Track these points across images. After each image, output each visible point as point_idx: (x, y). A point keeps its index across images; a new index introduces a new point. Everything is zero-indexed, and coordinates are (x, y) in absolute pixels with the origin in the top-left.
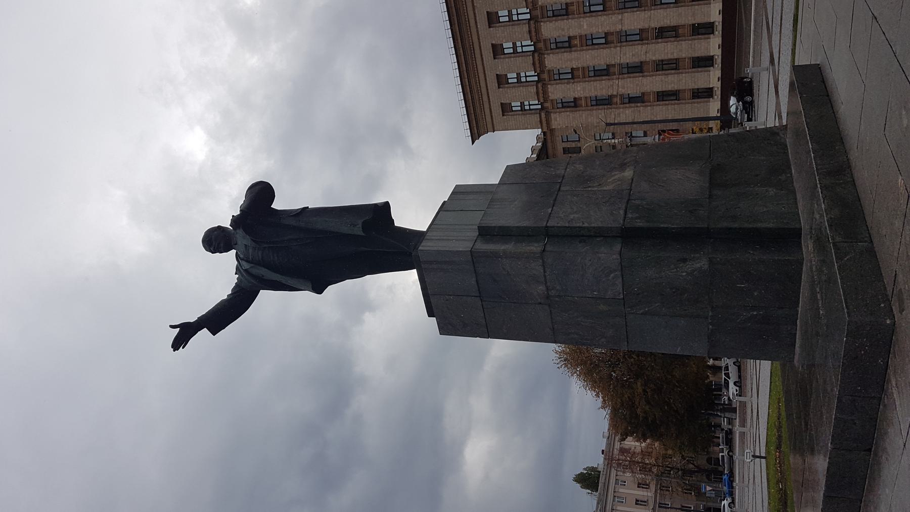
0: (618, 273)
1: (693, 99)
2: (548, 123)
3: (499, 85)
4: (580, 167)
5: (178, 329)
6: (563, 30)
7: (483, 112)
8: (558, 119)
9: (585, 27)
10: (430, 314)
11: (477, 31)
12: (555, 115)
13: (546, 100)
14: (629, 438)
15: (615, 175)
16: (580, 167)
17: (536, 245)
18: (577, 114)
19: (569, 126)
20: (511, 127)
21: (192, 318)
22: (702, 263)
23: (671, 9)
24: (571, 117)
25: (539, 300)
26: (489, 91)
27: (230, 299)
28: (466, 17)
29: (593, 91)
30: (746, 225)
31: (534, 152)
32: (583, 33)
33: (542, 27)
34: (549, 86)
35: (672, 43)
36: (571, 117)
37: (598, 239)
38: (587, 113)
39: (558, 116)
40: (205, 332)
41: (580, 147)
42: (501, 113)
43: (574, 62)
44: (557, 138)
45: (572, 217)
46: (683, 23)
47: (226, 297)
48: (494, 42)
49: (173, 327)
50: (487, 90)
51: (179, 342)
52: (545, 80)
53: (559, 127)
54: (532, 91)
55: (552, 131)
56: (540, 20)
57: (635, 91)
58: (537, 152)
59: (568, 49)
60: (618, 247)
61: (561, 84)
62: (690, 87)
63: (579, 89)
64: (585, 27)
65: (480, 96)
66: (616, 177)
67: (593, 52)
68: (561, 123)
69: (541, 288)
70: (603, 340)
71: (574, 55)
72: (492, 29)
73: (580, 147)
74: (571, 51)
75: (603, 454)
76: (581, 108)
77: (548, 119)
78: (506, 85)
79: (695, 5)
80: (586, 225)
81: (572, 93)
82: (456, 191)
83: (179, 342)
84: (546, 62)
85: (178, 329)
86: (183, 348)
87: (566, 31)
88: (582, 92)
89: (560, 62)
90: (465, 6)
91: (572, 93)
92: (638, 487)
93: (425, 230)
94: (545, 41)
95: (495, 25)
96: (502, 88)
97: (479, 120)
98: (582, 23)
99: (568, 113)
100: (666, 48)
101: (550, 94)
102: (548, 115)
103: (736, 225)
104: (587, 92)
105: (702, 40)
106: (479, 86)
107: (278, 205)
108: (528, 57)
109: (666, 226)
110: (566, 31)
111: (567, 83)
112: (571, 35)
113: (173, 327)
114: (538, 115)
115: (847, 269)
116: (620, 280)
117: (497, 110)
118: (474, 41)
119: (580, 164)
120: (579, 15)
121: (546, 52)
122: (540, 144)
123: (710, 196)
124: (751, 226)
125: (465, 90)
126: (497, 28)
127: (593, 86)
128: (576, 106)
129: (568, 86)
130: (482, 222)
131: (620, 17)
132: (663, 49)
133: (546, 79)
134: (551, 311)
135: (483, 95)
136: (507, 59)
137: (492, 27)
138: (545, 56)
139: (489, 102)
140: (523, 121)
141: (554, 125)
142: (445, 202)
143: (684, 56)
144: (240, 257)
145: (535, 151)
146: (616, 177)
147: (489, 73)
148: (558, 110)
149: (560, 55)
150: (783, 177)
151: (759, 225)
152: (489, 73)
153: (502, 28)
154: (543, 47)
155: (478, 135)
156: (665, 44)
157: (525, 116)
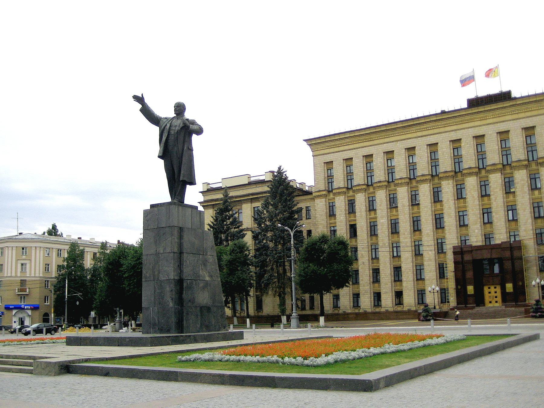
0: (167, 279)
1: (395, 291)
4: (211, 260)
6: (380, 205)
7: (326, 148)
8: (321, 204)
9: (381, 221)
10: (152, 206)
11: (382, 144)
12: (324, 201)
15: (207, 274)
16: (211, 260)
17: (177, 250)
18: (324, 217)
19: (316, 212)
20: (316, 169)
21: (146, 101)
22: (171, 305)
23: (390, 278)
24: (323, 213)
25: (158, 250)
26: (341, 153)
27: (155, 117)
28: (391, 136)
29: (340, 228)
30: (184, 318)
31: (300, 185)
32: (378, 219)
33: (383, 191)
34: (344, 196)
35: (369, 280)
36: (323, 213)
38: (325, 224)
39: (323, 203)
41: (302, 220)
43: (359, 213)
44: (308, 203)
46: (381, 286)
48: (374, 156)
49: (142, 95)
50: (342, 151)
51: (136, 98)
53: (316, 205)
54: (341, 184)
55: (313, 199)
56: (387, 189)
57: (187, 291)
58: (301, 187)
59: (368, 209)
60: (176, 278)
61: (345, 205)
62: (340, 293)
64: (381, 221)
67: (365, 227)
68: (318, 206)
69: (162, 251)
70: (145, 273)
71: (364, 214)
72: (383, 154)
73: (302, 220)
74: (366, 211)
75: (79, 238)
76: (328, 220)
77: (322, 197)
78: (345, 165)
79: (392, 293)
80: (184, 267)
81: (339, 213)
82: (201, 212)
83: (136, 98)
84: (360, 194)
87: (380, 208)
88: (339, 220)
89: (360, 204)
90: (398, 134)
91: (339, 213)
94: (374, 193)
95: (385, 156)
96: (343, 162)
98: (384, 218)
99: (325, 211)
100: (366, 276)
101: (338, 197)
103: (184, 314)
104: (340, 224)
105: (370, 299)
107: (194, 136)
108: (363, 181)
109: (184, 293)
110: (380, 208)
111: (345, 209)
112: (377, 211)
113: (142, 95)
114: (324, 189)
116: (165, 279)
118: (375, 141)
120: (389, 216)
121: (367, 194)
122: (307, 188)
123: (196, 307)
124: (184, 319)
126: (383, 158)
127: (343, 227)
128: (330, 216)
129: (344, 210)
131: (387, 244)
132: (365, 274)
135: (338, 148)
136: (362, 165)
137: (384, 154)
138: (364, 193)
139: (334, 153)
140: (320, 178)
141: (317, 201)
143: (361, 288)
145: (302, 185)
147: (353, 152)
148: (328, 203)
149: (364, 204)
150: (204, 329)
151: (185, 321)
152: (353, 152)
153: (383, 162)
154: (371, 191)
156: (368, 276)
157: (324, 179)
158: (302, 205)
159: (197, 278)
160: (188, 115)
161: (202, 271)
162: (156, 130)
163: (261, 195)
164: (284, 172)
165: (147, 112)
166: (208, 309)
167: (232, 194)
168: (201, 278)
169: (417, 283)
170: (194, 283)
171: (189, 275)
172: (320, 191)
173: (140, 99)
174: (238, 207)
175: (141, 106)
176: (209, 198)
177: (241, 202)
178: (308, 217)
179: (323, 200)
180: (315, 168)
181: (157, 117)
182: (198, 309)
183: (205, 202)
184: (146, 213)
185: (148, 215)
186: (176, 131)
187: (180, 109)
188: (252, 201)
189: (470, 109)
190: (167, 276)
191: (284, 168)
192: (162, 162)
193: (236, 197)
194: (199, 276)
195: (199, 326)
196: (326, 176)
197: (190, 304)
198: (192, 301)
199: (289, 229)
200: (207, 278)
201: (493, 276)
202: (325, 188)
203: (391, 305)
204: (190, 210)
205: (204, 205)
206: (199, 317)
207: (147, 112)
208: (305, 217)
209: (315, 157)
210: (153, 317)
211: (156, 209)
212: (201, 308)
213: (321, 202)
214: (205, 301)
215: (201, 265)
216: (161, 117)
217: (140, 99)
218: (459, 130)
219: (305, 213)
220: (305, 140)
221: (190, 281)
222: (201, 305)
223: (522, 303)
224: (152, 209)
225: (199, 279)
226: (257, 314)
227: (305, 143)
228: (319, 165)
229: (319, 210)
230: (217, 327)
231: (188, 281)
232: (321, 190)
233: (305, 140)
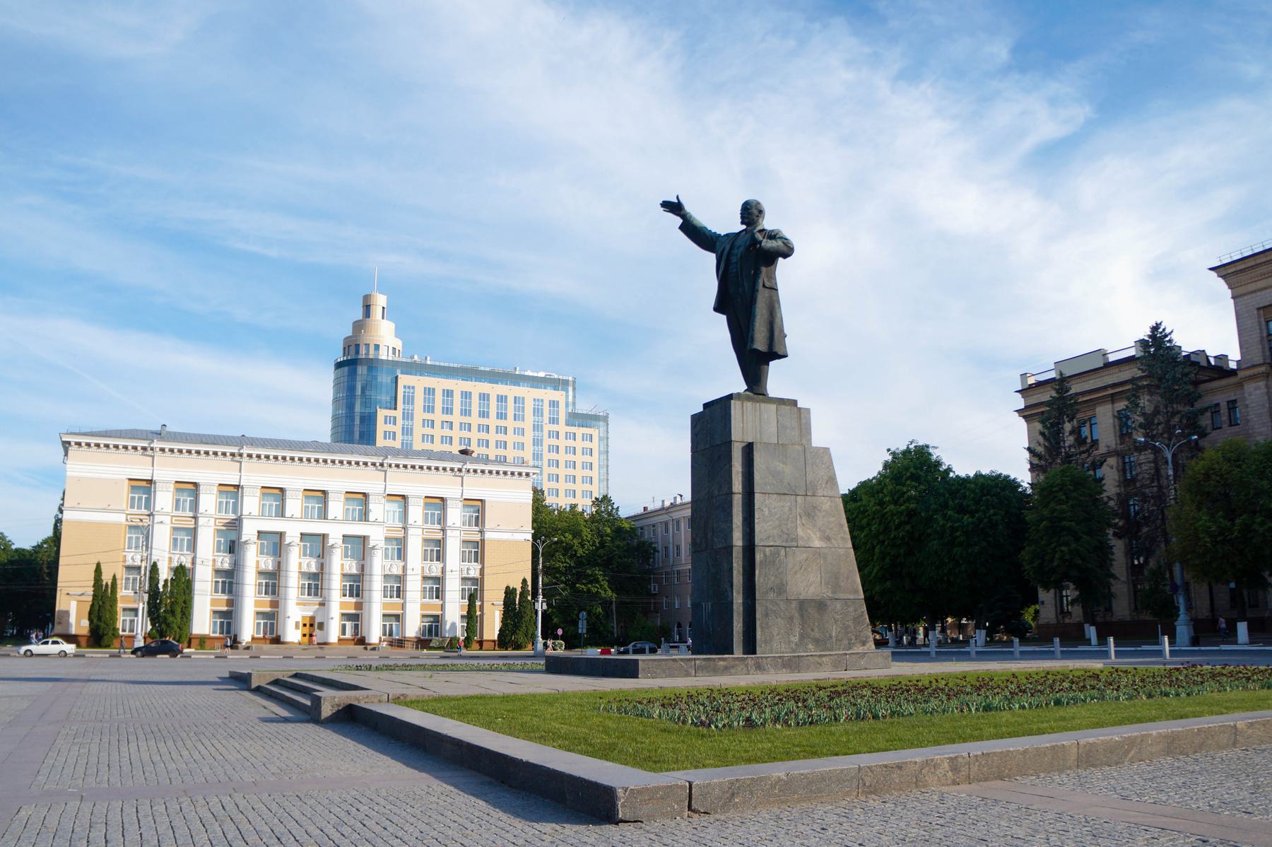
2: (1252, 378)
5: (677, 201)
8: (1258, 392)
10: (706, 406)
12: (1263, 387)
15: (815, 534)
21: (689, 208)
40: (679, 221)
42: (1261, 305)
44: (1233, 394)
49: (678, 198)
55: (1240, 385)
78: (1263, 319)
85: (677, 201)
96: (1258, 314)
97: (1246, 275)
102: (1263, 376)
113: (678, 198)
114: (1262, 361)
115: (828, 739)
119: (831, 507)
125: (1230, 266)
130: (758, 444)
141: (1249, 387)
155: (1224, 276)
158: (1222, 399)
159: (790, 543)
160: (768, 223)
161: (803, 530)
162: (711, 258)
163: (1120, 389)
164: (1166, 336)
165: (692, 230)
166: (821, 605)
167: (1075, 388)
168: (801, 543)
169: (193, 546)
170: (783, 552)
171: (769, 537)
172: (1254, 366)
173: (674, 207)
174: (1089, 413)
175: (681, 221)
176: (1033, 400)
177: (1093, 403)
178: (1233, 421)
179: (1262, 384)
180: (1240, 321)
181: (712, 237)
182: (794, 605)
183: (1027, 407)
184: (696, 419)
186: (739, 255)
187: (750, 213)
188: (1113, 398)
191: (1168, 326)
192: (722, 319)
193: (1083, 393)
194: (795, 540)
195: (796, 639)
196: (1265, 335)
197: (771, 596)
198: (781, 589)
200: (817, 543)
202: (1264, 359)
203: (1127, 612)
205: (1026, 414)
206: (797, 621)
207: (692, 230)
208: (1228, 421)
209: (1238, 300)
210: (453, 625)
212: (802, 604)
213: (1256, 389)
214: (812, 590)
215: (801, 517)
216: (720, 235)
217: (674, 207)
219: (1227, 414)
220: (1211, 269)
221: (772, 548)
222: (801, 597)
223: (946, 650)
224: (707, 410)
225: (795, 544)
226: (1136, 617)
227: (1214, 274)
228: (1246, 315)
229: (1253, 405)
230: (845, 642)
231: (767, 549)
232: (1255, 363)
233: (1211, 269)
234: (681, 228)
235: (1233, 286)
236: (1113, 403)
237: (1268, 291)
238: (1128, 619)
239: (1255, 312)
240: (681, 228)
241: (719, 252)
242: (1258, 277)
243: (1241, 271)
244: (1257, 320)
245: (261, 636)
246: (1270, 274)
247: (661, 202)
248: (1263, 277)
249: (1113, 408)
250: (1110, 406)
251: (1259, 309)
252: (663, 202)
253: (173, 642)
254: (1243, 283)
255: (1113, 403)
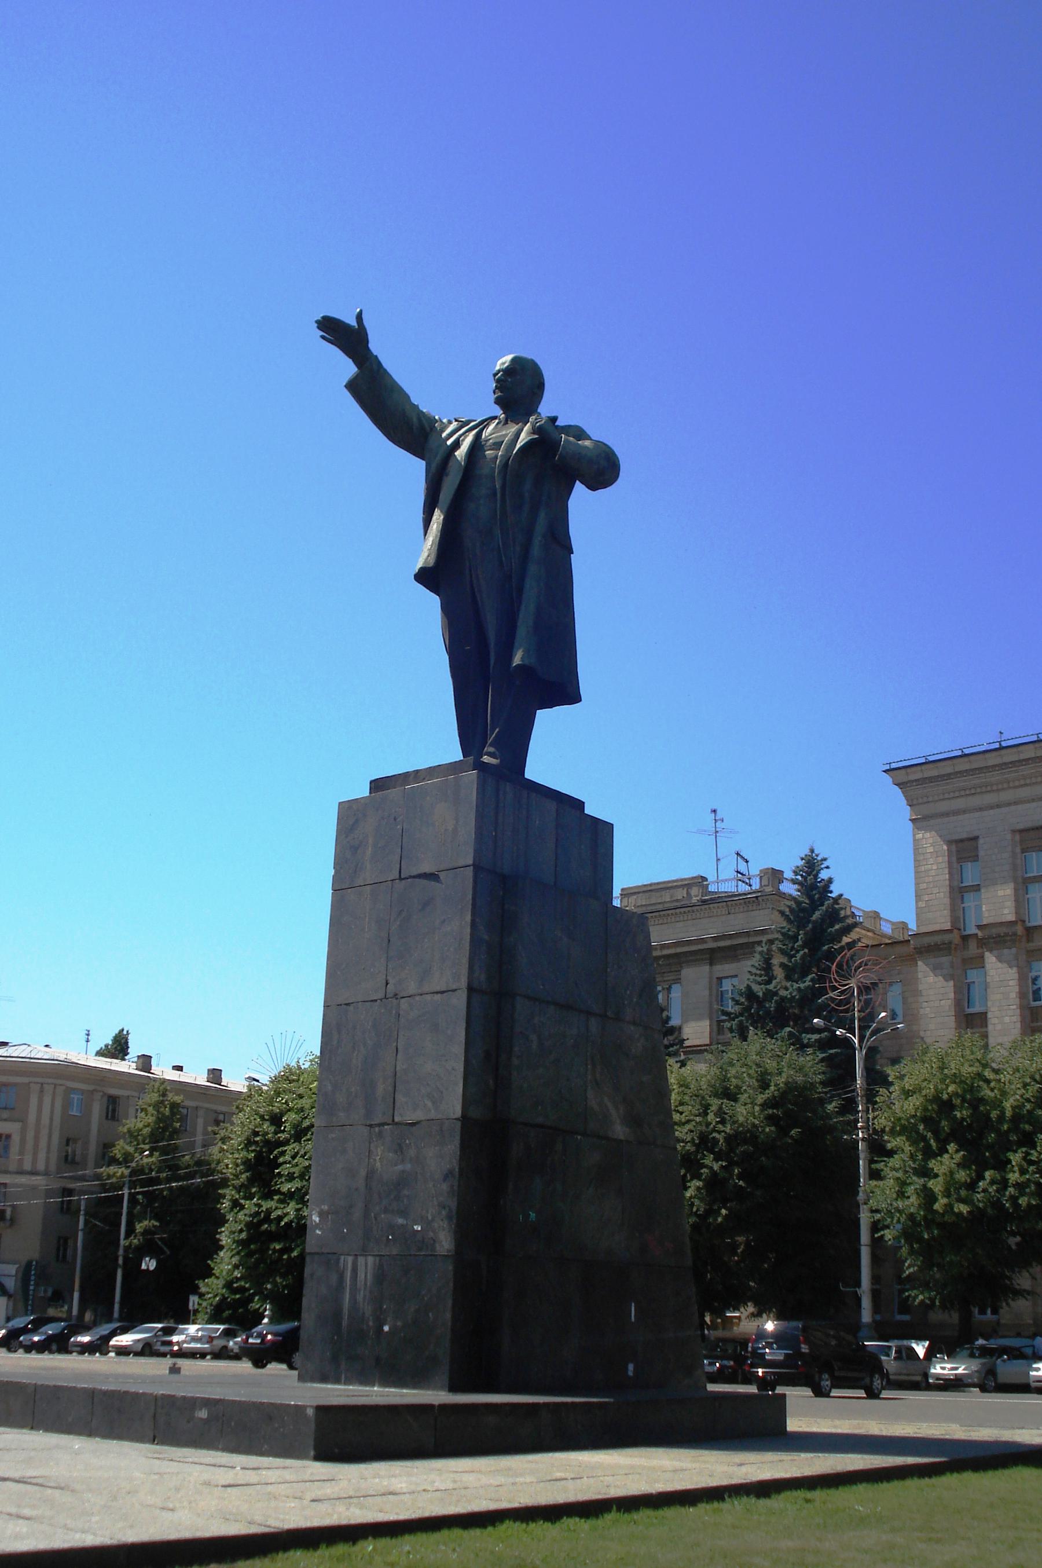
3: (1021, 831)
13: (982, 943)
14: (778, 1388)
17: (483, 977)
21: (376, 346)
37: (491, 1082)
40: (348, 368)
45: (534, 1037)
47: (415, 401)
49: (359, 317)
52: (1028, 941)
54: (1006, 911)
63: (1007, 1019)
65: (995, 788)
66: (613, 1112)
69: (412, 988)
80: (515, 1061)
86: (323, 337)
92: (59, 1238)
93: (526, 777)
106: (1034, 780)
107: (580, 496)
113: (359, 317)
117: (965, 826)
133: (1031, 944)
134: (376, 1001)
142: (579, 805)
144: (482, 430)
146: (613, 1112)
185: (357, 821)
189: (212, 1361)
190: (429, 1104)
192: (431, 603)
199: (851, 1036)
200: (620, 1131)
201: (366, 1255)
204: (551, 806)
211: (393, 793)
218: (969, 997)
227: (887, 779)
234: (352, 386)
235: (915, 802)
236: (711, 964)
237: (967, 816)
238: (913, 1341)
239: (1009, 836)
240: (352, 386)
241: (438, 459)
242: (960, 791)
243: (931, 779)
244: (946, 858)
245: (342, 1257)
246: (1039, 779)
247: (319, 317)
248: (963, 793)
249: (711, 972)
250: (707, 968)
251: (1014, 831)
252: (324, 318)
253: (121, 1252)
254: (930, 799)
255: (711, 964)
